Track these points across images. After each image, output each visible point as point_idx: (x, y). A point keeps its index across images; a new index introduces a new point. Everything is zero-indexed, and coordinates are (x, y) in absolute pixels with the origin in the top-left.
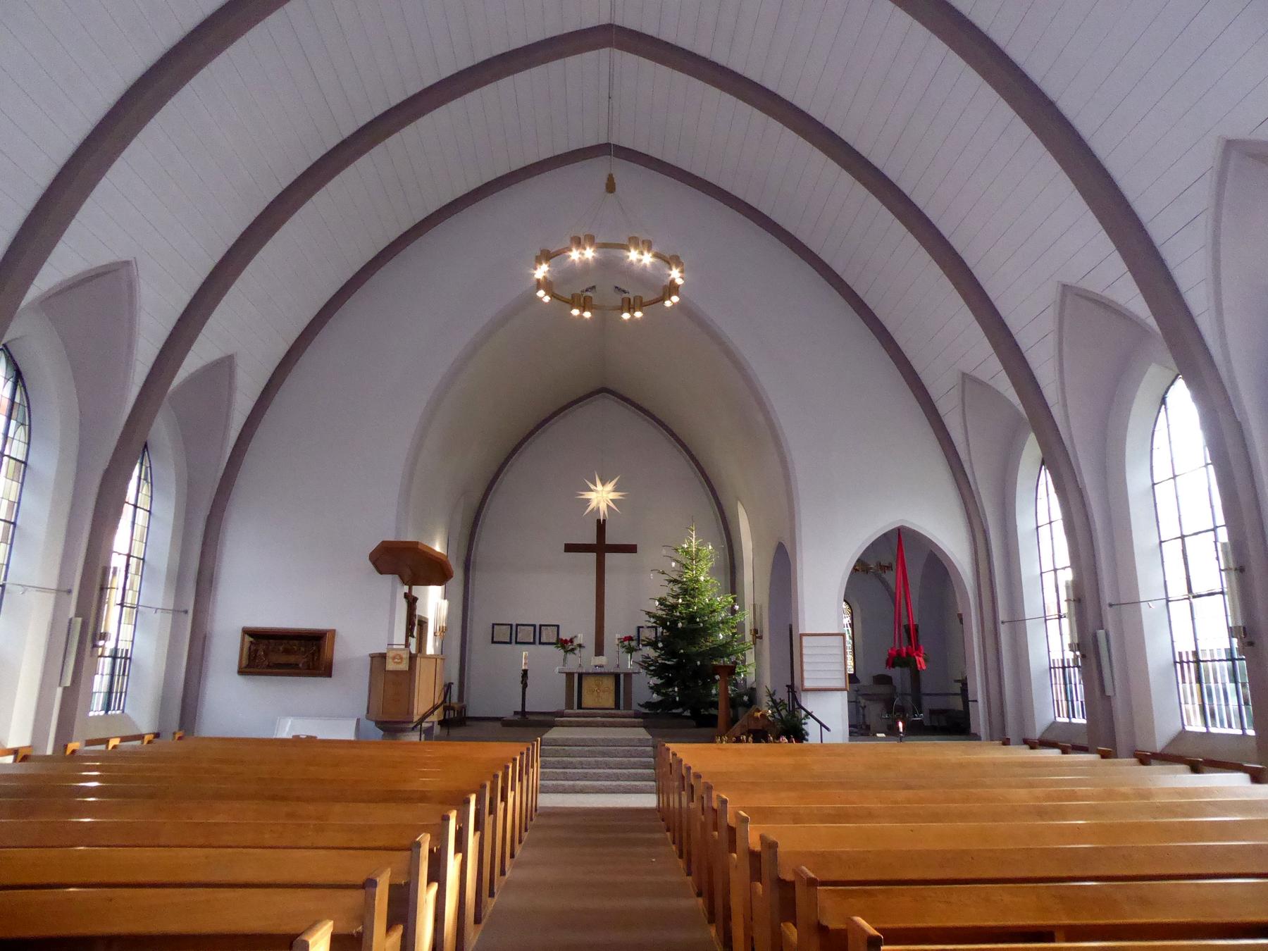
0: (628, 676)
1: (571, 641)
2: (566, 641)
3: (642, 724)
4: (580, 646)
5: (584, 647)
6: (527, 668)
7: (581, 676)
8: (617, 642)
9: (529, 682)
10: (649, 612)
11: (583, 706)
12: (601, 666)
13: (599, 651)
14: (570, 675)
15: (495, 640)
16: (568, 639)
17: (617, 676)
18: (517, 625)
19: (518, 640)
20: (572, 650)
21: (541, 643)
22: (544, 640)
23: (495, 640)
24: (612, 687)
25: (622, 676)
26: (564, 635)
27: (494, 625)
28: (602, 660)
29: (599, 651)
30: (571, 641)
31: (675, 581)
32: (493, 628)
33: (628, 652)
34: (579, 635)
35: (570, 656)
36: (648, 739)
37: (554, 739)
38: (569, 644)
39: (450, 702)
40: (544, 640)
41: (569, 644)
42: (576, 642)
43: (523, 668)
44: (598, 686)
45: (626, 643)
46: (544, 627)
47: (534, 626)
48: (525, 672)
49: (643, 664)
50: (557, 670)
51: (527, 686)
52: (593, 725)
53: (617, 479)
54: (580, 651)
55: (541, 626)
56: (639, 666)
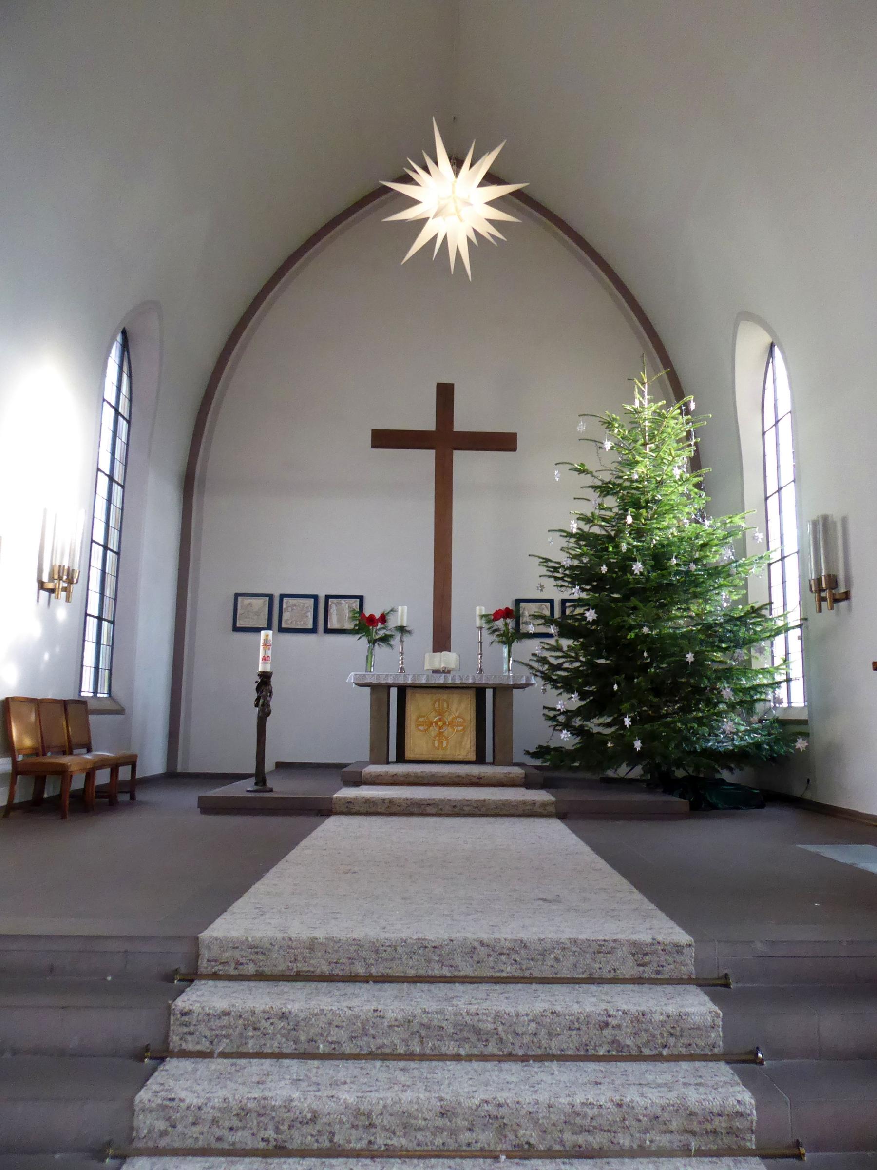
0: (503, 691)
1: (383, 619)
2: (372, 620)
3: (552, 809)
4: (402, 629)
5: (409, 632)
6: (268, 668)
7: (402, 690)
8: (478, 622)
9: (273, 703)
10: (547, 560)
11: (409, 755)
12: (446, 671)
13: (442, 642)
14: (379, 690)
15: (239, 624)
16: (377, 616)
17: (479, 692)
18: (282, 596)
19: (284, 625)
20: (385, 639)
21: (327, 631)
22: (333, 624)
23: (239, 624)
24: (470, 715)
25: (489, 693)
26: (372, 609)
27: (237, 595)
28: (448, 659)
29: (442, 642)
30: (383, 619)
31: (605, 489)
32: (494, 760)
33: (504, 643)
34: (400, 608)
35: (381, 650)
36: (678, 948)
37: (256, 949)
38: (380, 625)
39: (789, 702)
40: (333, 624)
41: (380, 625)
42: (393, 622)
43: (260, 669)
44: (440, 713)
45: (500, 623)
46: (335, 600)
47: (316, 598)
48: (265, 679)
49: (535, 665)
50: (351, 678)
51: (269, 714)
52: (429, 810)
53: (473, 144)
54: (402, 641)
55: (328, 597)
56: (526, 671)
